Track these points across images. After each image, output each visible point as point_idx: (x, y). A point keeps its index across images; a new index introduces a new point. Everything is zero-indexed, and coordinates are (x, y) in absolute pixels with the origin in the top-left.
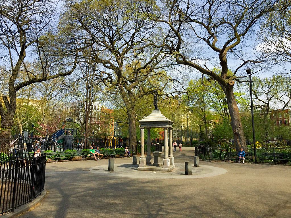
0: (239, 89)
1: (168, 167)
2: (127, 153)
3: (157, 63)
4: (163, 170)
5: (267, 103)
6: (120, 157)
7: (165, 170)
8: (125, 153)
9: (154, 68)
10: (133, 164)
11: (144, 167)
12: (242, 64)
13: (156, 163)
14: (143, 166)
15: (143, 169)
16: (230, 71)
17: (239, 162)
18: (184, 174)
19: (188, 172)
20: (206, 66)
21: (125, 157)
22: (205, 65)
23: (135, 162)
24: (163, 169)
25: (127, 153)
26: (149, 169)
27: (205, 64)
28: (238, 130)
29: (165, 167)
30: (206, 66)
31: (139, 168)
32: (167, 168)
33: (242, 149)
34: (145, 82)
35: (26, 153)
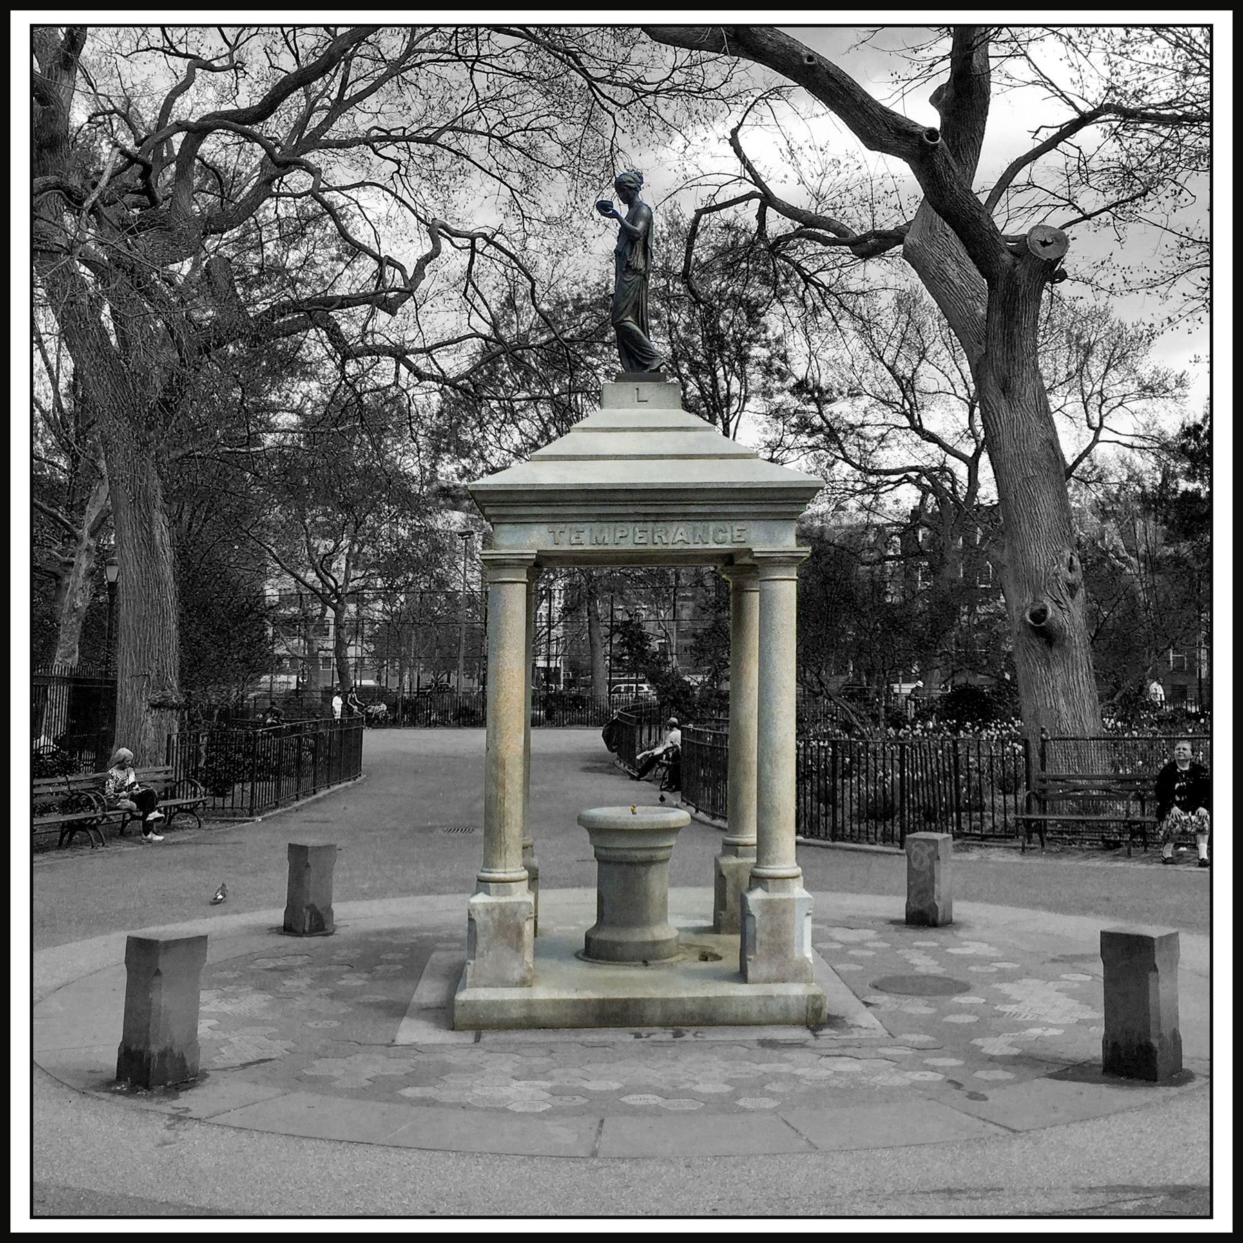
0: (814, 363)
1: (800, 973)
2: (129, 803)
3: (340, 106)
4: (754, 1016)
5: (970, 455)
6: (60, 846)
7: (775, 1008)
9: (315, 142)
10: (288, 929)
11: (523, 983)
12: (1045, 135)
13: (628, 924)
14: (516, 975)
15: (516, 1013)
17: (1168, 854)
18: (1074, 1071)
19: (1155, 1042)
20: (738, 151)
22: (734, 142)
24: (745, 1001)
26: (585, 1003)
27: (734, 132)
28: (1057, 602)
30: (738, 151)
32: (797, 990)
33: (1187, 745)
35: (410, 424)
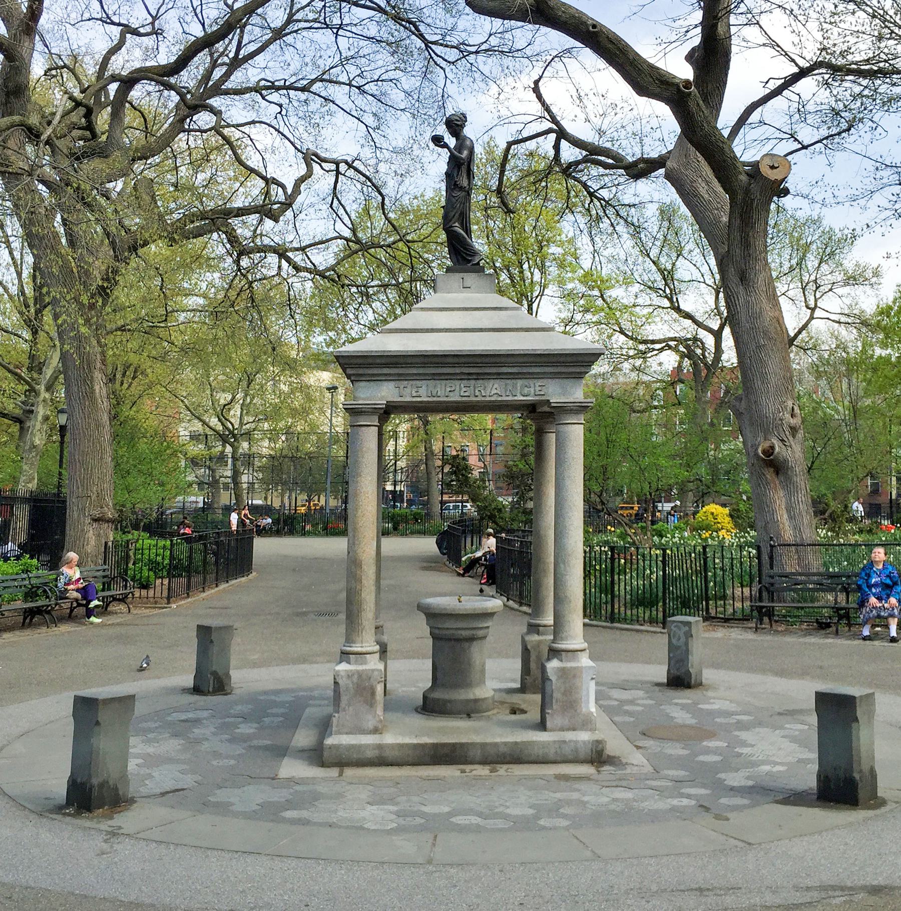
1: (587, 724)
2: (76, 595)
3: (236, 63)
4: (552, 756)
6: (23, 626)
7: (567, 750)
8: (63, 595)
9: (217, 90)
10: (197, 690)
11: (376, 731)
12: (773, 85)
15: (370, 754)
16: (285, 348)
18: (795, 798)
19: (857, 776)
20: (539, 97)
21: (62, 619)
22: (536, 90)
23: (215, 674)
24: (544, 745)
25: (76, 595)
26: (416, 746)
27: (536, 83)
29: (566, 722)
30: (539, 97)
31: (337, 747)
32: (584, 736)
34: (114, 230)
